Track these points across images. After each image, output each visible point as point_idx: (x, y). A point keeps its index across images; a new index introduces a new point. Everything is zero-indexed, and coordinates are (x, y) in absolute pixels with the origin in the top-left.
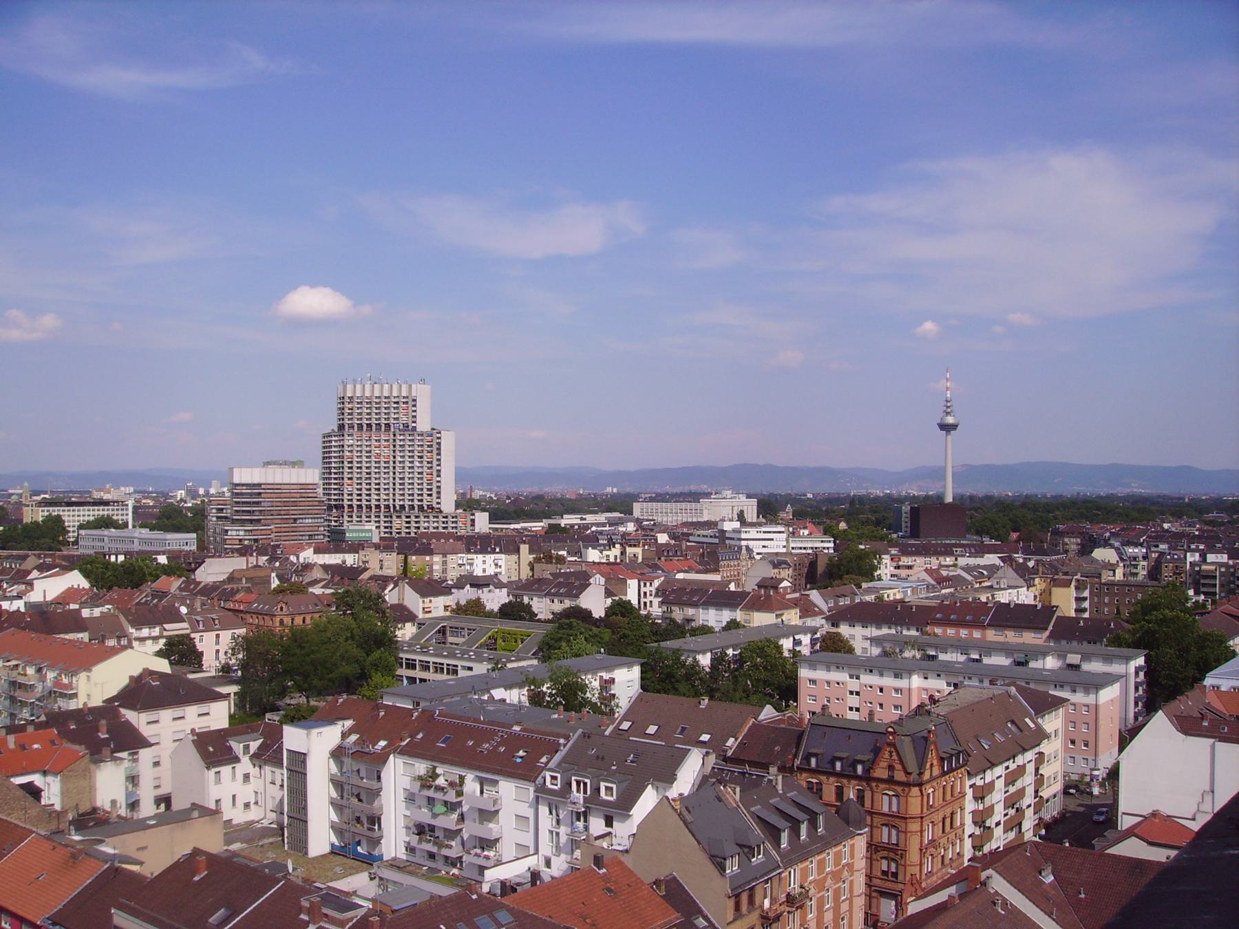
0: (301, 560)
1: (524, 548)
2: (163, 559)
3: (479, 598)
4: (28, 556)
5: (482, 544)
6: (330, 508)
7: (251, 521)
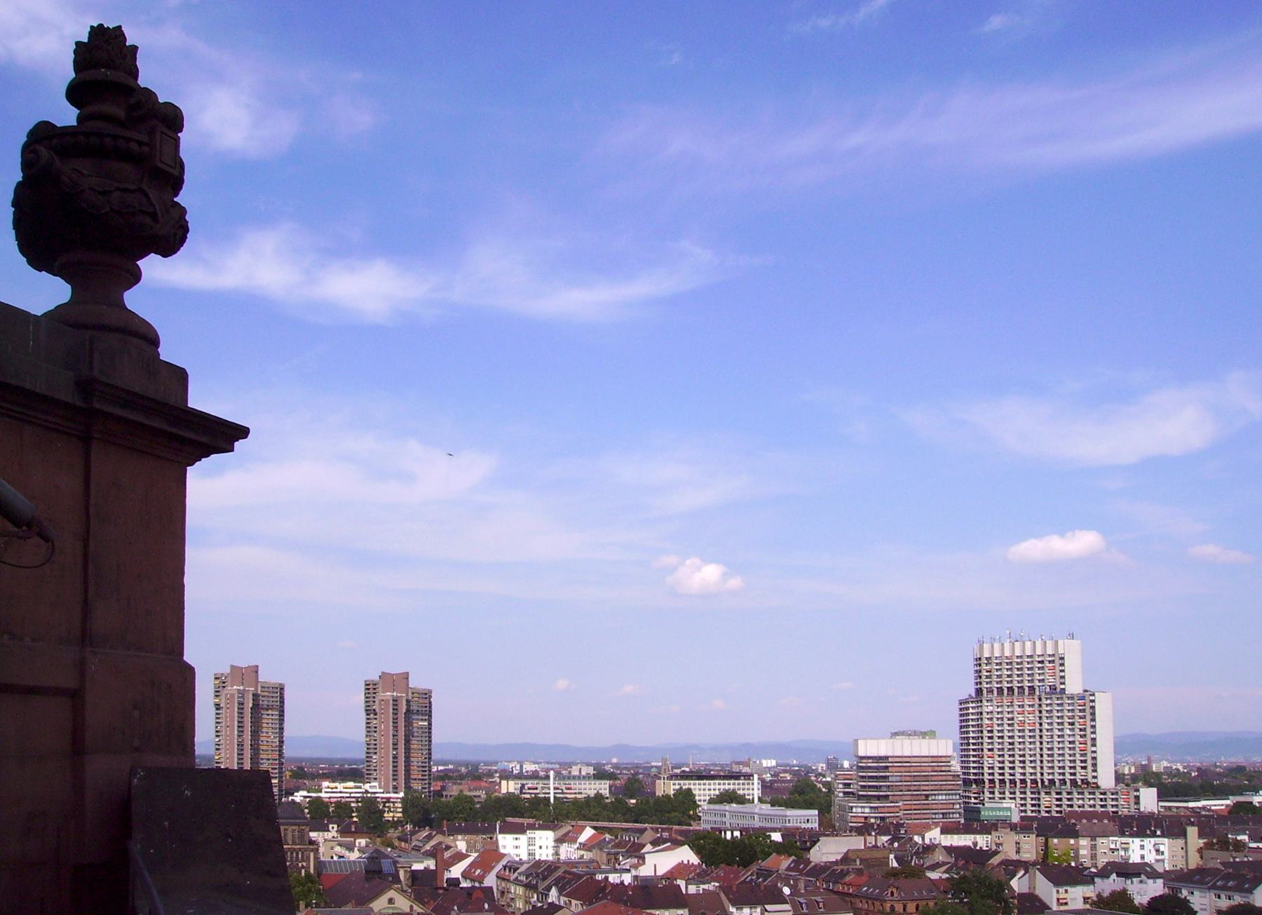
0: (927, 841)
1: (1192, 831)
2: (776, 837)
3: (1124, 891)
4: (646, 829)
5: (1141, 825)
6: (967, 783)
7: (878, 798)
